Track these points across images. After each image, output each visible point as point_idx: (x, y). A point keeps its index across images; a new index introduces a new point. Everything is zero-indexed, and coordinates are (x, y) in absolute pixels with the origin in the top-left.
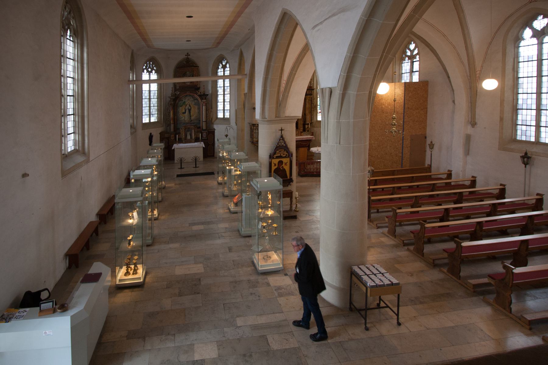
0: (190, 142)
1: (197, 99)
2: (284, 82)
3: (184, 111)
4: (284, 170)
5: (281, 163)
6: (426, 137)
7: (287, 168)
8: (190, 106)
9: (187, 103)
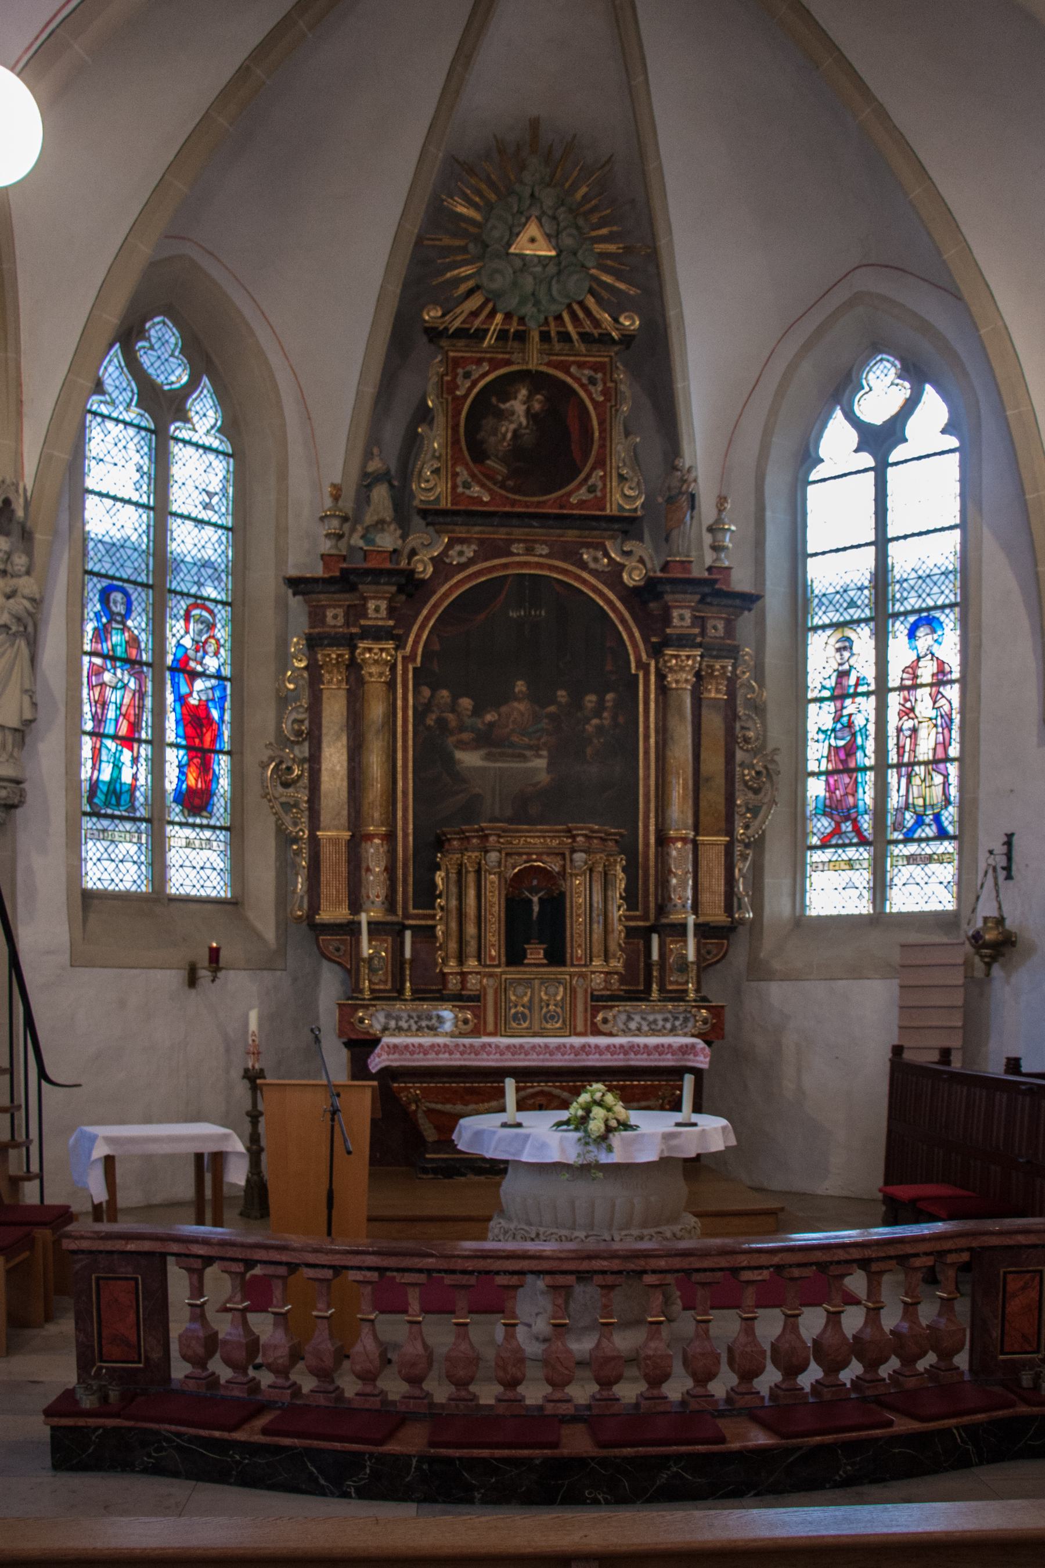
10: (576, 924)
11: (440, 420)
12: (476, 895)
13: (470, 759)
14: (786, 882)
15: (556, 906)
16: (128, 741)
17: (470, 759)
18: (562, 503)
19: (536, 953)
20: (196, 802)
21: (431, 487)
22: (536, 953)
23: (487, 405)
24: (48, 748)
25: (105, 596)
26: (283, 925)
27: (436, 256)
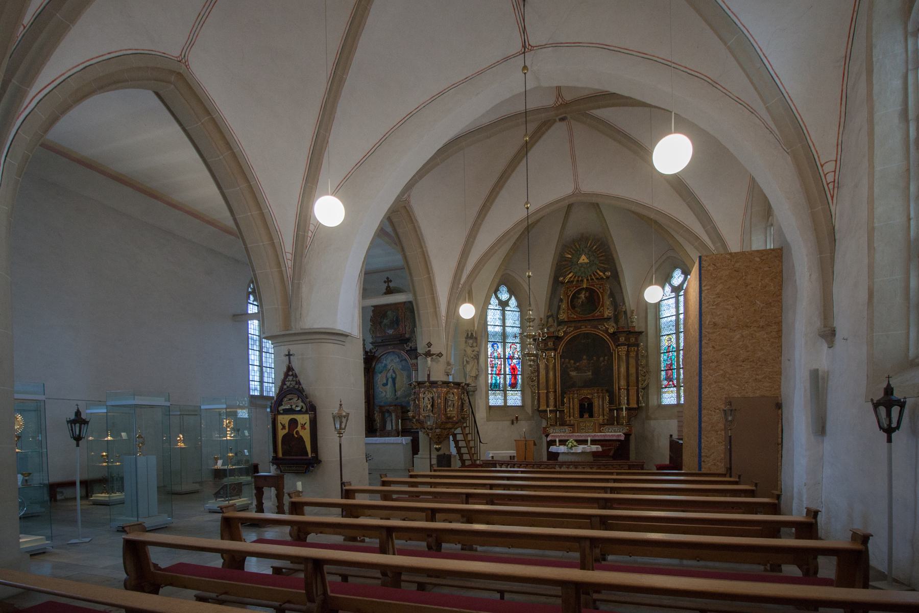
0: (388, 435)
1: (405, 360)
2: (289, 256)
3: (385, 381)
4: (301, 439)
5: (293, 423)
6: (779, 406)
7: (306, 435)
8: (394, 372)
9: (389, 367)
10: (596, 409)
11: (565, 301)
12: (572, 403)
13: (573, 374)
14: (655, 397)
15: (591, 405)
16: (498, 374)
17: (573, 374)
18: (576, 328)
19: (586, 415)
20: (513, 385)
21: (563, 316)
22: (586, 415)
23: (575, 296)
24: (482, 379)
25: (493, 346)
26: (533, 411)
27: (561, 267)
